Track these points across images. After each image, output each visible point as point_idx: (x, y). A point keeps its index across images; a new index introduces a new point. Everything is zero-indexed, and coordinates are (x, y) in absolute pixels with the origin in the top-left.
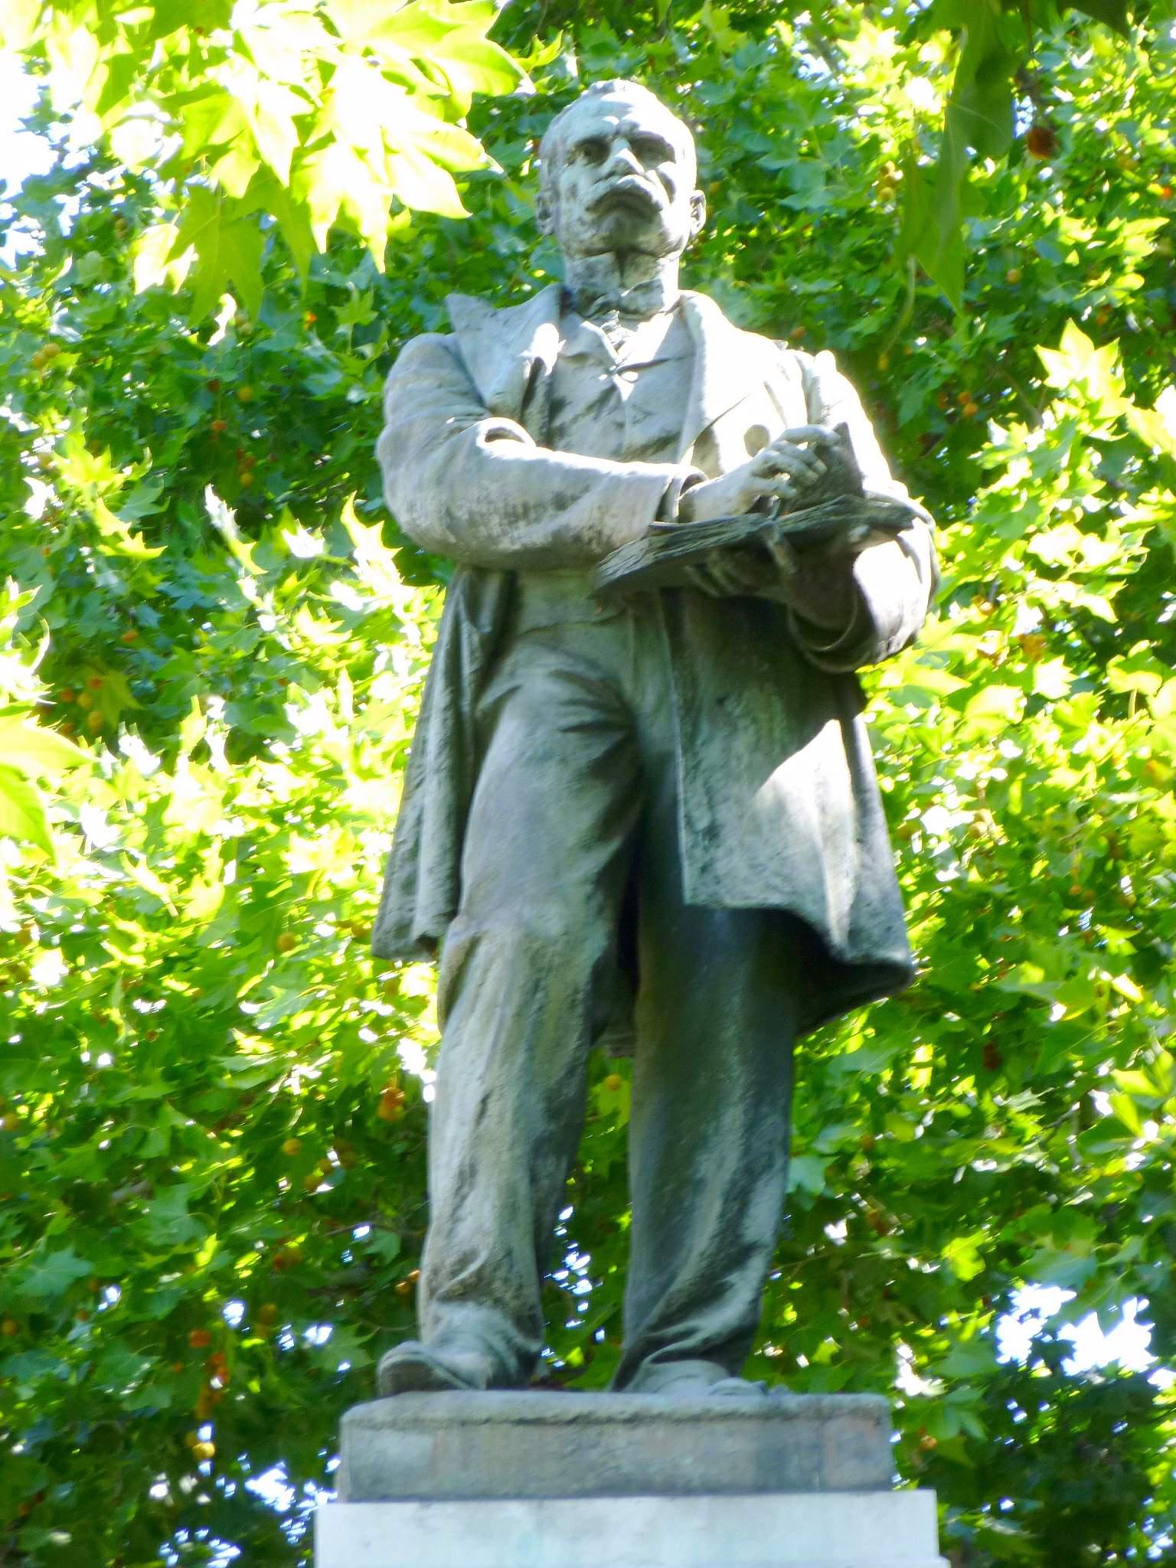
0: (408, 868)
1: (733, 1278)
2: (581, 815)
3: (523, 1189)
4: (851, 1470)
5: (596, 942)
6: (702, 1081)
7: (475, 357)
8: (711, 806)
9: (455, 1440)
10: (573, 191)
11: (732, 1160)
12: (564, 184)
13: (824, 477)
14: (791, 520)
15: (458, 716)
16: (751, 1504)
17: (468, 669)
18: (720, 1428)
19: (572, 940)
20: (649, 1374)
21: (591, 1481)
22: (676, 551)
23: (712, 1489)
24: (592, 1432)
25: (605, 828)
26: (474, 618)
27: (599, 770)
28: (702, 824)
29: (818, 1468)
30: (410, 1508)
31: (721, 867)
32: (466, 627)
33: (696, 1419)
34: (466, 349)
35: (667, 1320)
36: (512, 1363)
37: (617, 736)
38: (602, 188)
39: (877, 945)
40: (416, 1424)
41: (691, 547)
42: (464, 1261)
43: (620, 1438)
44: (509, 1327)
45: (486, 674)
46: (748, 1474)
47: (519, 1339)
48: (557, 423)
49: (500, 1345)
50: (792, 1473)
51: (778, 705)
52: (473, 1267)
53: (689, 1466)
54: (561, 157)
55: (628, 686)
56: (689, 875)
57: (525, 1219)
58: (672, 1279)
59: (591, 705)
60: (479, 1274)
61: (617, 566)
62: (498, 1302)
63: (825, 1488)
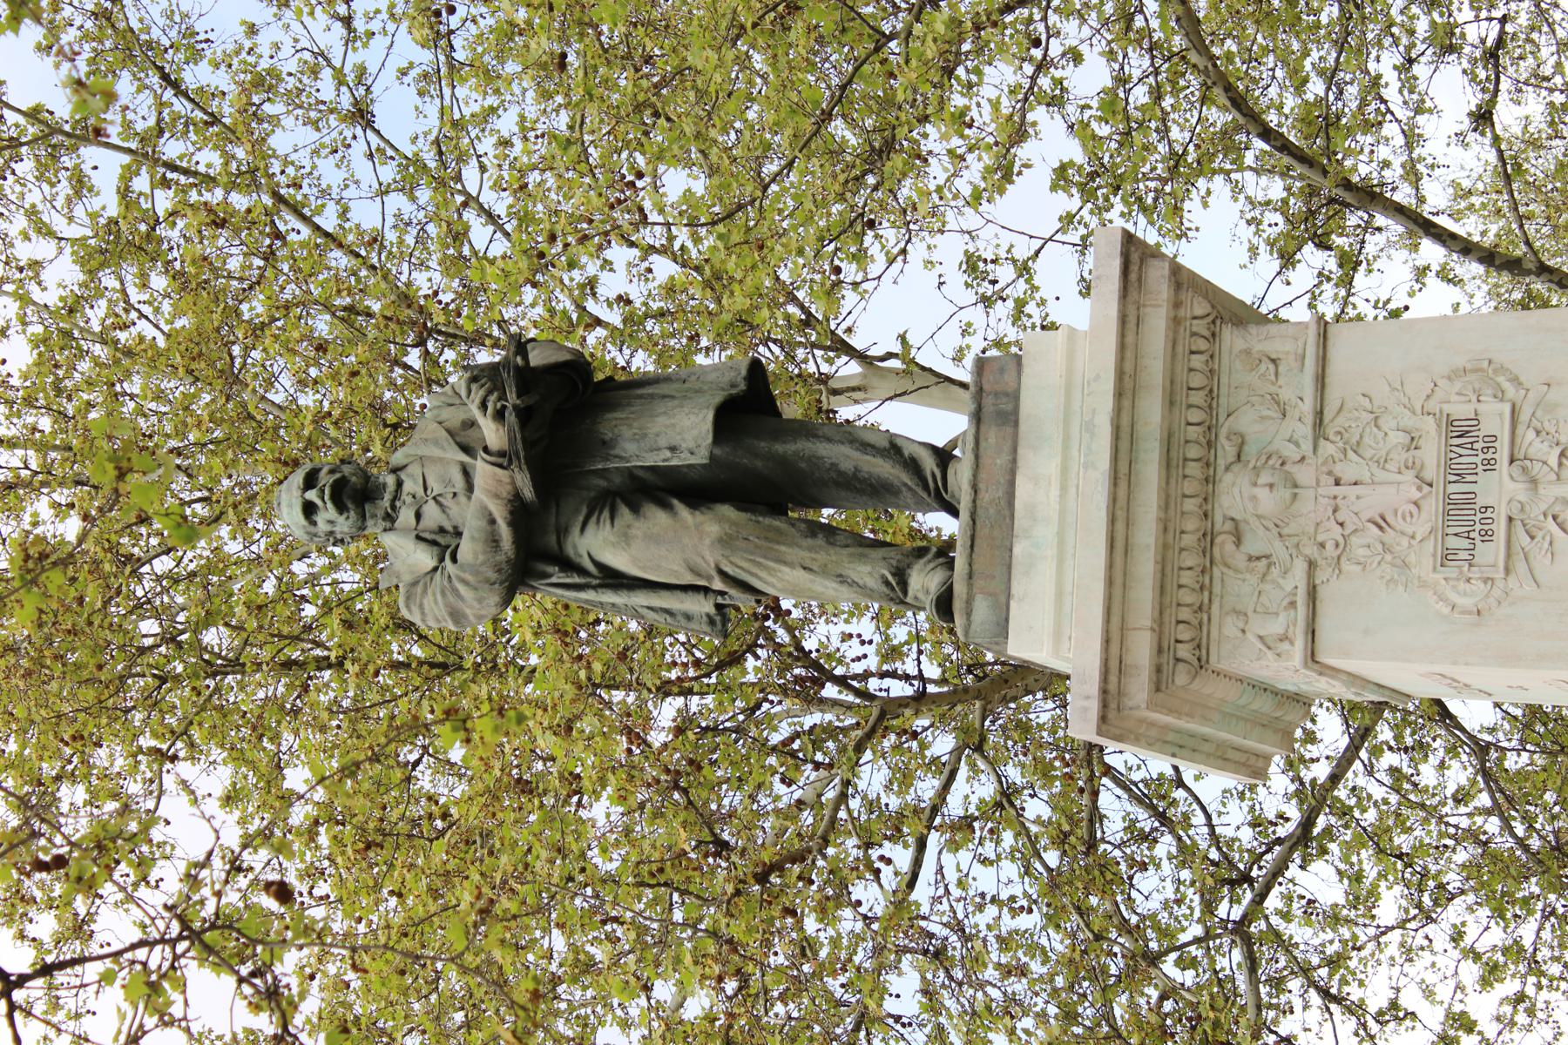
0: (680, 618)
1: (906, 453)
2: (657, 518)
3: (851, 550)
4: (1010, 377)
5: (727, 510)
6: (803, 465)
7: (412, 572)
8: (659, 449)
9: (978, 583)
10: (331, 522)
11: (845, 450)
12: (328, 528)
13: (490, 379)
14: (512, 397)
15: (600, 586)
16: (1023, 427)
17: (576, 580)
18: (983, 444)
19: (721, 520)
20: (953, 496)
21: (1007, 512)
22: (522, 454)
23: (1015, 450)
24: (980, 512)
25: (666, 506)
26: (550, 576)
27: (635, 509)
28: (668, 454)
29: (1007, 395)
30: (1013, 604)
31: (692, 445)
32: (554, 580)
33: (977, 457)
34: (408, 577)
35: (926, 487)
36: (941, 560)
37: (618, 501)
38: (329, 505)
39: (738, 371)
40: (969, 602)
41: (520, 446)
42: (887, 583)
43: (985, 497)
44: (922, 561)
45: (582, 571)
46: (1009, 430)
47: (930, 556)
48: (450, 529)
49: (932, 565)
50: (1009, 407)
51: (609, 416)
52: (890, 578)
53: (1002, 460)
54: (312, 529)
55: (592, 494)
56: (693, 460)
57: (867, 551)
58: (905, 485)
59: (601, 513)
60: (894, 575)
61: (528, 493)
62: (909, 566)
63: (1018, 391)
